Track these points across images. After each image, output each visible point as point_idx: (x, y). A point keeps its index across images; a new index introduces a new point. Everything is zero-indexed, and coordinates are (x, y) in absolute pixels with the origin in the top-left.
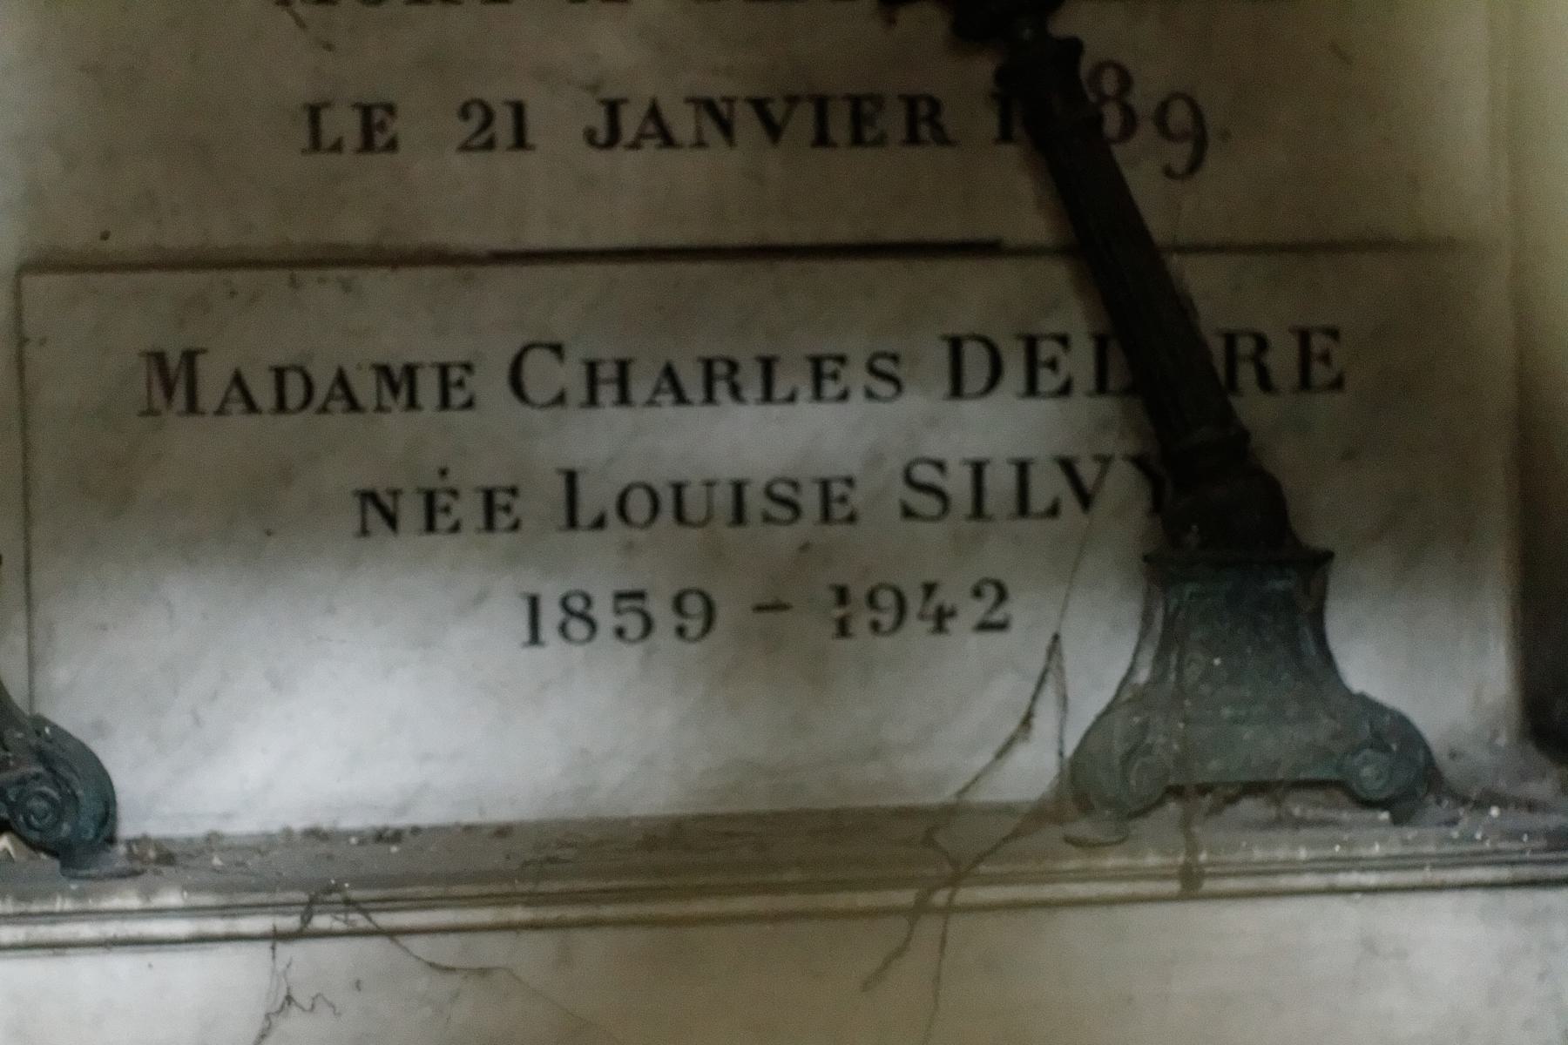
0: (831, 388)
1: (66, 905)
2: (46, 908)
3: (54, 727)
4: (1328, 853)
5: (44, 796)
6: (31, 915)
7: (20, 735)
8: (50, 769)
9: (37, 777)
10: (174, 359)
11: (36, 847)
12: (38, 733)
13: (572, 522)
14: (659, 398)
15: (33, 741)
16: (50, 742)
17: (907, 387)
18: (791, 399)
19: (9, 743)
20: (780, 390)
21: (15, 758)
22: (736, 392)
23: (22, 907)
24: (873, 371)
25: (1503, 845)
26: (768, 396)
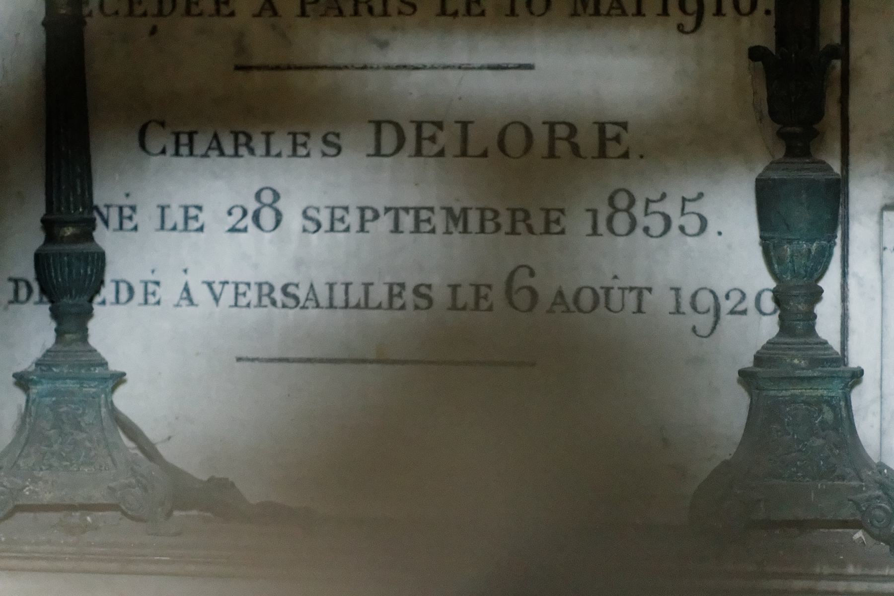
0: (302, 151)
1: (827, 570)
2: (880, 573)
3: (889, 469)
4: (103, 406)
5: (880, 507)
6: (873, 576)
7: (870, 473)
8: (886, 494)
9: (878, 497)
10: (457, 211)
11: (877, 538)
12: (880, 472)
13: (162, 228)
14: (210, 152)
15: (878, 477)
16: (887, 478)
17: (344, 149)
18: (279, 155)
19: (864, 477)
20: (274, 151)
21: (866, 486)
22: (252, 151)
23: (867, 571)
24: (325, 141)
25: (71, 385)
26: (268, 153)
